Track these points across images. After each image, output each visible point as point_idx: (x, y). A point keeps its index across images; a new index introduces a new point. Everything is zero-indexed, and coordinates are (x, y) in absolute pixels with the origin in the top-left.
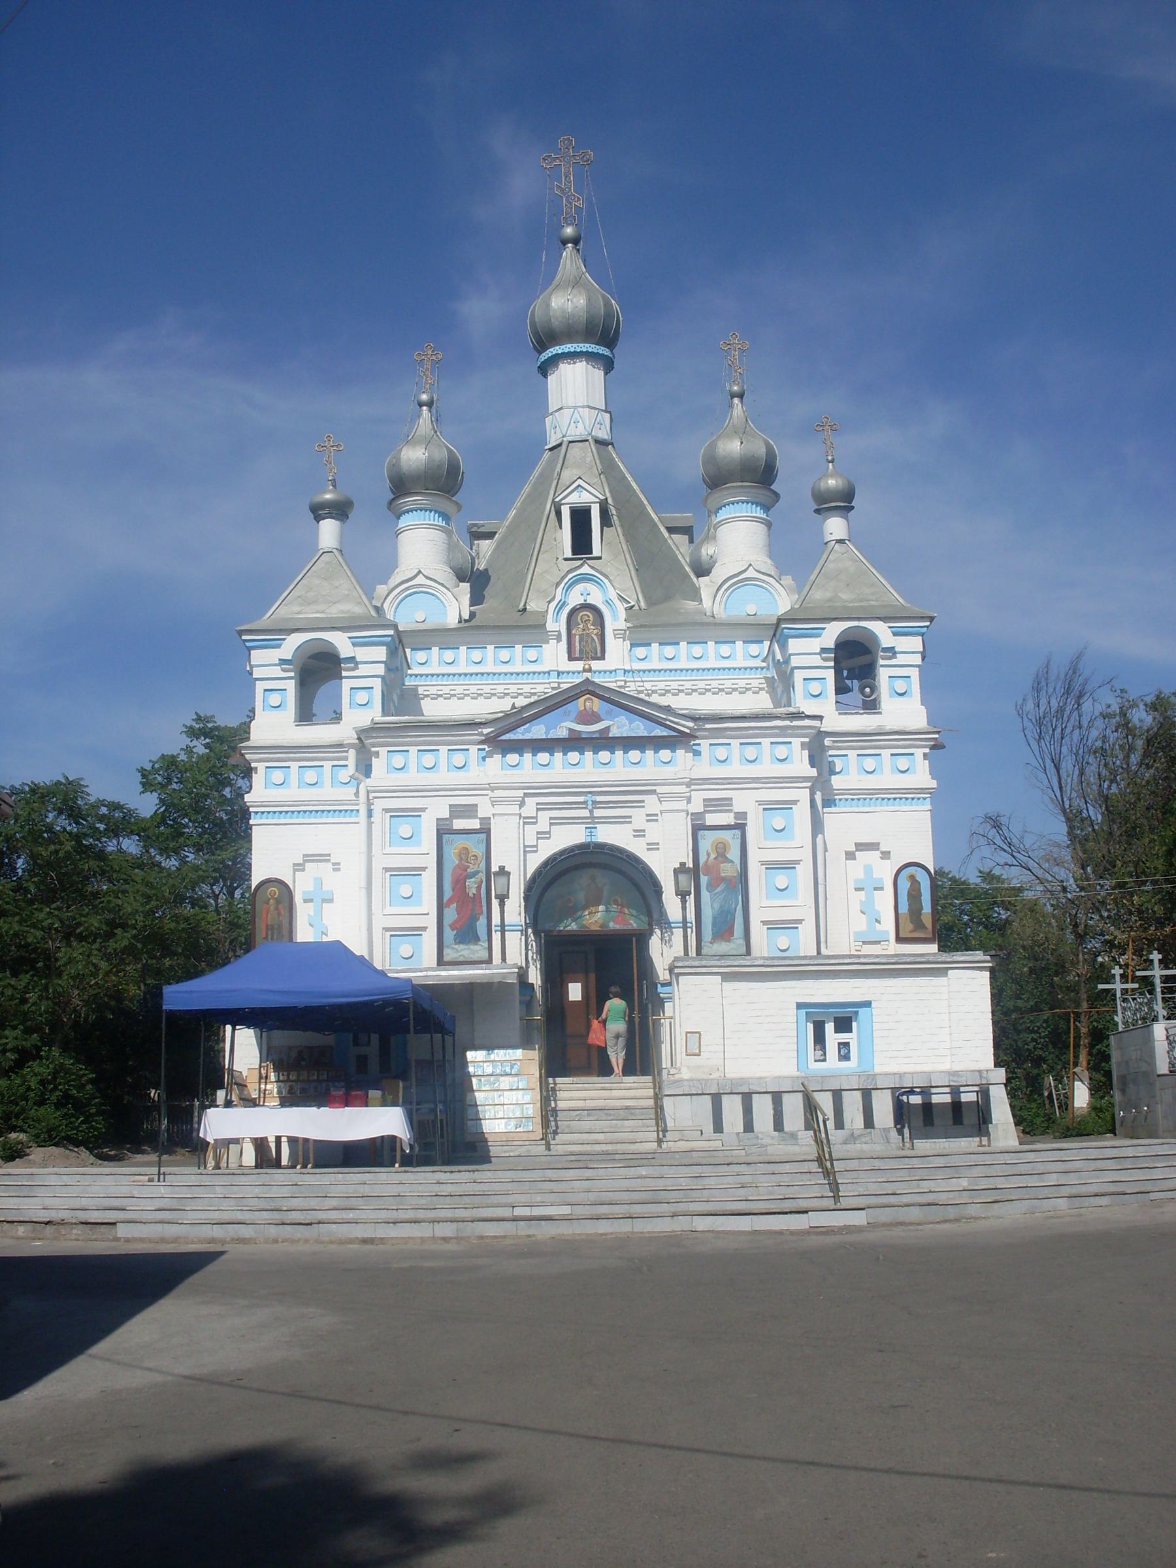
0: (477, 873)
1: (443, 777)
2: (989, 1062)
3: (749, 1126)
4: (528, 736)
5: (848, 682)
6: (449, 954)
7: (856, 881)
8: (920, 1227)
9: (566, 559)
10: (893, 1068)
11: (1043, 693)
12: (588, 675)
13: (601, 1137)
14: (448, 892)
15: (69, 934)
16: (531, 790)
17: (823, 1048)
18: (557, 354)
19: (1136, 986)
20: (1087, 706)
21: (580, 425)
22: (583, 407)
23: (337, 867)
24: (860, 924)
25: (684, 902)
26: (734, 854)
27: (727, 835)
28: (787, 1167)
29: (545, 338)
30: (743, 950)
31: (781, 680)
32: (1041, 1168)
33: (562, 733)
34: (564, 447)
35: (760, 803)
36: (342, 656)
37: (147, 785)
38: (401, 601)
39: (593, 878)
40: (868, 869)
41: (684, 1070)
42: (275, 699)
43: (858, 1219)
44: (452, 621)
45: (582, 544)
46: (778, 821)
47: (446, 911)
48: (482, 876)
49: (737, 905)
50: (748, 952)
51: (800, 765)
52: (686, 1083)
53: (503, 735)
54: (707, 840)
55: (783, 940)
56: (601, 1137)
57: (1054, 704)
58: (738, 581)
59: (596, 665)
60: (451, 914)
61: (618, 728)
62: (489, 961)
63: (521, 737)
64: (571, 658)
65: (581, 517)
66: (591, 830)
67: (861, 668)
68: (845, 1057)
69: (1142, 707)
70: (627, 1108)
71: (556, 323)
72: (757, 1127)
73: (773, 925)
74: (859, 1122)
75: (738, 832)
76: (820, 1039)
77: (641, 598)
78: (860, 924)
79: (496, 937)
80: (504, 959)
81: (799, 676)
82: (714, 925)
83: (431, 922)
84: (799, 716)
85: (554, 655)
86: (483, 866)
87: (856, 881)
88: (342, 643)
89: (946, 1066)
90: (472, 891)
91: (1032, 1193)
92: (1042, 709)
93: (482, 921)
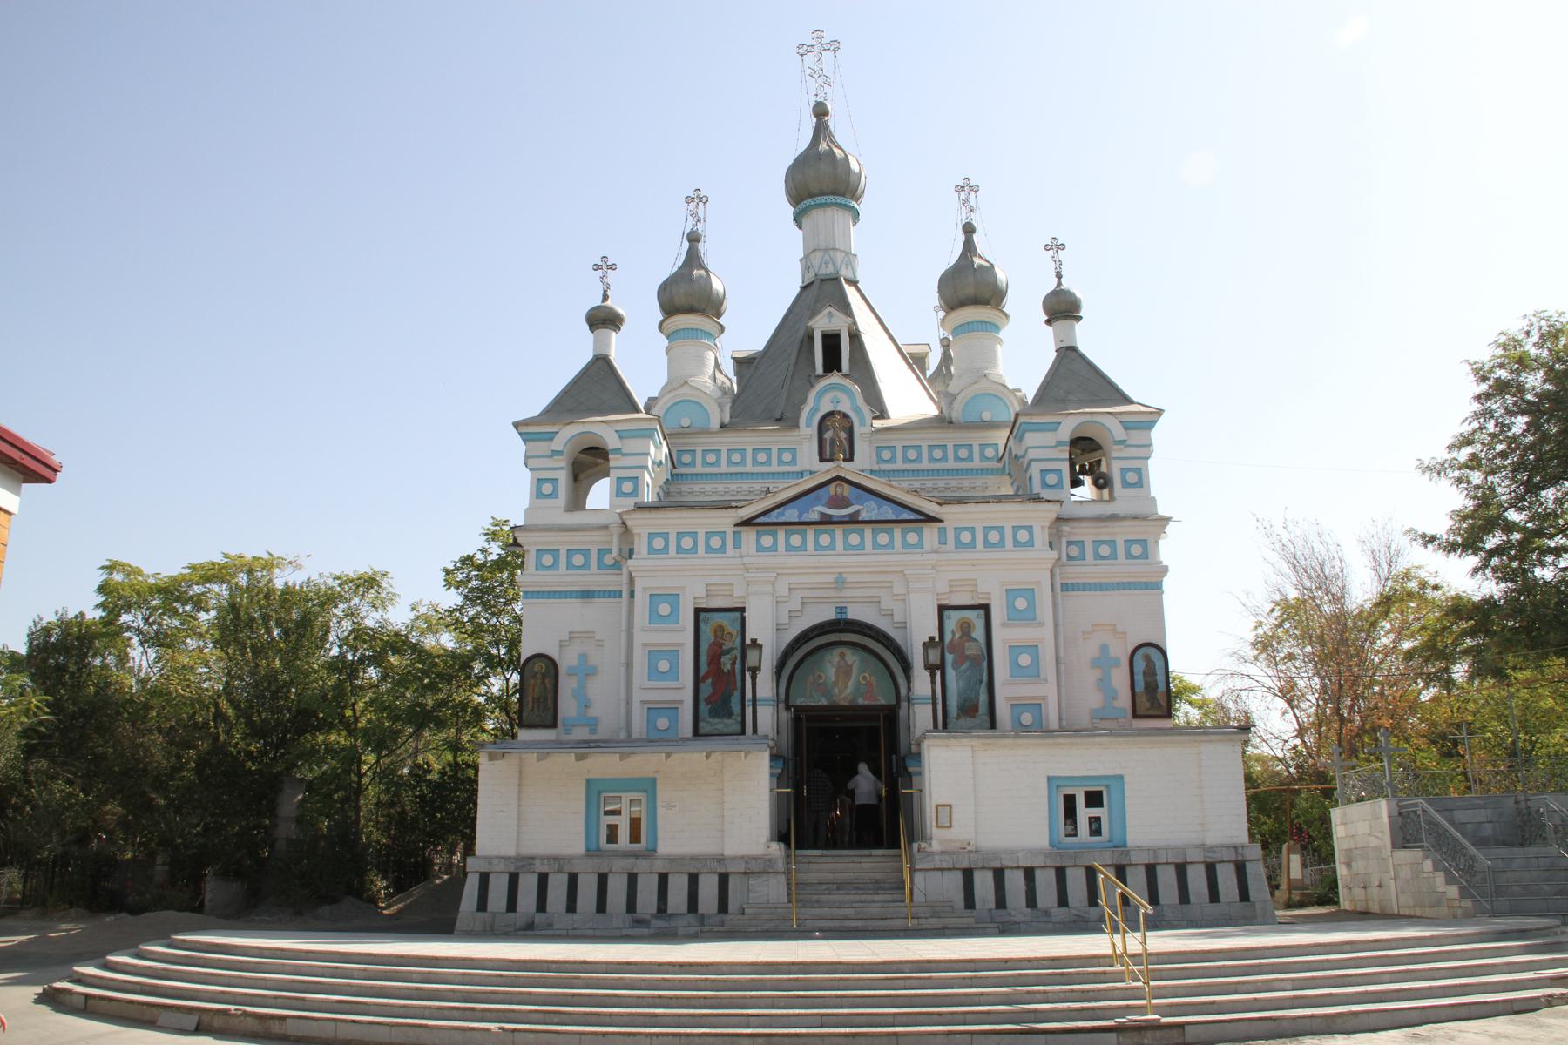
2: (1244, 838)
14: (704, 668)
17: (1075, 823)
26: (978, 633)
27: (970, 615)
39: (842, 656)
48: (737, 653)
81: (1035, 470)
86: (738, 641)
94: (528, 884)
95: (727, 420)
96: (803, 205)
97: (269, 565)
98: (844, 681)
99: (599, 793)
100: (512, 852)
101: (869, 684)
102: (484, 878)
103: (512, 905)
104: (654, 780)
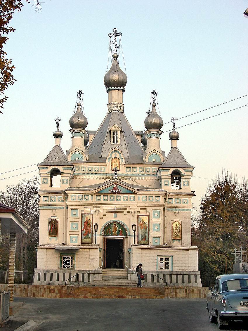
1: (83, 201)
2: (197, 270)
13: (115, 282)
25: (134, 232)
31: (159, 180)
34: (112, 113)
44: (85, 160)
45: (116, 141)
51: (162, 201)
56: (115, 282)
60: (84, 232)
62: (92, 243)
64: (112, 171)
70: (121, 276)
72: (198, 282)
75: (147, 217)
79: (94, 238)
81: (163, 180)
84: (163, 190)
94: (48, 275)
95: (88, 159)
96: (110, 88)
100: (44, 268)
102: (39, 274)
103: (45, 280)
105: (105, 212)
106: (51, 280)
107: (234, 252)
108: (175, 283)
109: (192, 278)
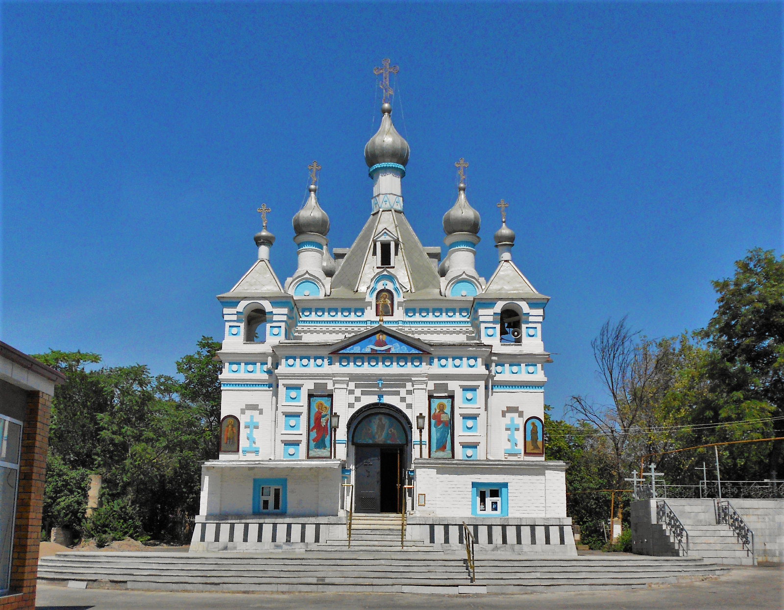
0: (326, 415)
3: (447, 541)
4: (352, 352)
5: (507, 329)
6: (312, 454)
7: (506, 425)
8: (512, 596)
9: (378, 268)
10: (518, 515)
11: (605, 337)
12: (381, 323)
13: (376, 543)
14: (312, 425)
15: (138, 438)
16: (353, 377)
17: (484, 504)
18: (378, 168)
19: (644, 480)
20: (627, 344)
21: (388, 203)
22: (390, 194)
23: (261, 413)
24: (508, 446)
25: (421, 432)
26: (448, 410)
27: (445, 401)
28: (453, 563)
29: (372, 158)
30: (450, 456)
32: (578, 569)
33: (368, 350)
35: (461, 386)
36: (267, 311)
37: (180, 370)
38: (300, 284)
39: (380, 420)
40: (512, 419)
41: (417, 512)
42: (234, 330)
43: (483, 590)
46: (469, 395)
47: (311, 433)
48: (328, 417)
49: (448, 434)
50: (453, 457)
51: (481, 369)
52: (418, 519)
53: (338, 353)
54: (435, 403)
55: (470, 452)
56: (376, 543)
57: (611, 342)
58: (458, 280)
59: (386, 318)
60: (314, 434)
61: (395, 348)
63: (348, 352)
64: (377, 315)
65: (386, 247)
66: (380, 397)
67: (514, 323)
68: (496, 509)
69: (654, 344)
71: (377, 152)
73: (465, 446)
74: (500, 541)
75: (450, 400)
76: (483, 501)
77: (412, 287)
78: (508, 446)
80: (335, 457)
81: (483, 326)
82: (437, 443)
83: (304, 439)
85: (370, 314)
86: (329, 412)
87: (506, 425)
88: (267, 306)
89: (543, 515)
90: (323, 424)
91: (572, 582)
92: (604, 344)
93: (328, 437)
97: (79, 358)
98: (380, 433)
99: (260, 485)
101: (393, 434)
103: (217, 539)
104: (286, 480)
105: (358, 392)
106: (231, 539)
107: (631, 476)
108: (513, 545)
109: (554, 533)
